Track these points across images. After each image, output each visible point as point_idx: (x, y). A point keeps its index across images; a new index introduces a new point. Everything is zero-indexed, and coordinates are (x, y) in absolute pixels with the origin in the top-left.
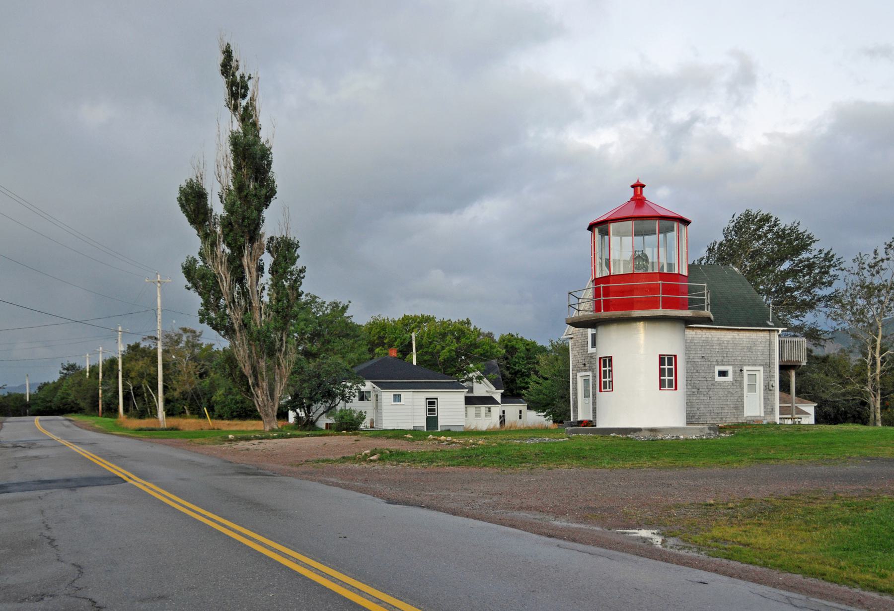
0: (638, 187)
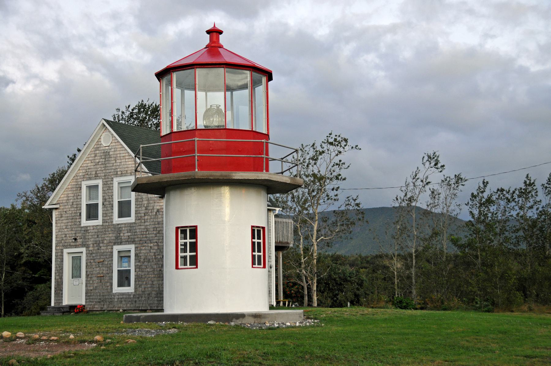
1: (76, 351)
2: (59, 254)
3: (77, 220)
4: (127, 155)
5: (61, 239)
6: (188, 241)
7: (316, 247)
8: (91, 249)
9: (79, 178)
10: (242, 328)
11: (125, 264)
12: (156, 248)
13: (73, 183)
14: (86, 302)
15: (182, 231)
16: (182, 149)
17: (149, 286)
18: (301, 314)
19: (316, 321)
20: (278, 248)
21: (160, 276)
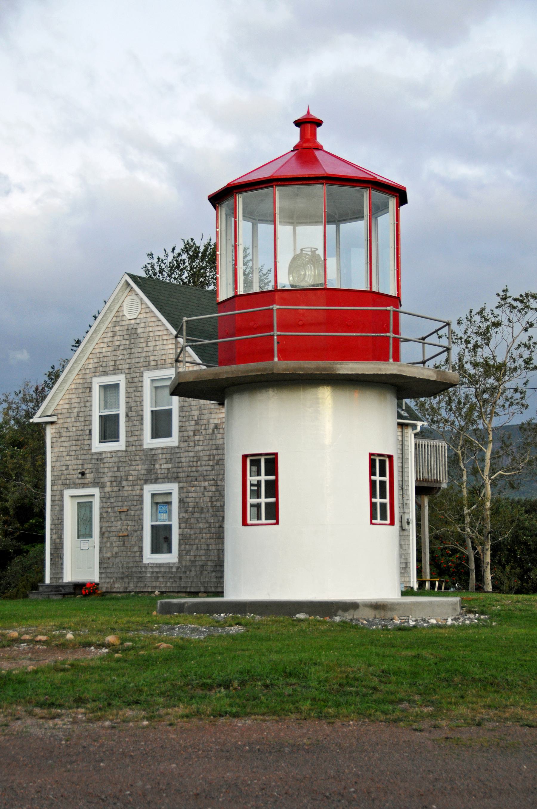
0: (308, 124)
1: (76, 660)
2: (57, 498)
3: (86, 442)
4: (165, 333)
5: (60, 473)
6: (263, 478)
7: (489, 488)
8: (108, 489)
9: (88, 371)
10: (352, 627)
11: (164, 516)
12: (213, 488)
13: (79, 381)
14: (100, 578)
15: (252, 461)
16: (252, 324)
17: (202, 552)
18: (455, 604)
19: (482, 617)
20: (420, 491)
21: (219, 535)
